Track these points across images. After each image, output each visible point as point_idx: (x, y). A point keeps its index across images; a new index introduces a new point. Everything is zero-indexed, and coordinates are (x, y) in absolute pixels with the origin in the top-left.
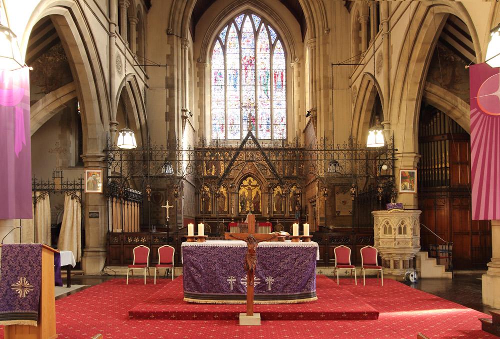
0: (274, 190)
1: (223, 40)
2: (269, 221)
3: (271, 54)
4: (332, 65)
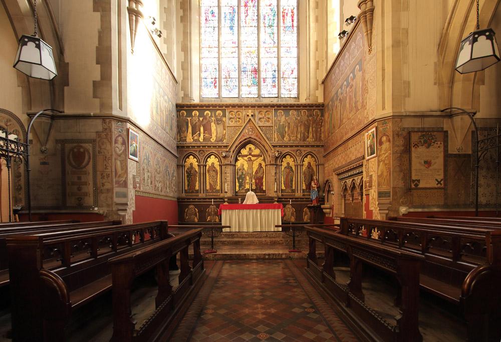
2: (278, 201)
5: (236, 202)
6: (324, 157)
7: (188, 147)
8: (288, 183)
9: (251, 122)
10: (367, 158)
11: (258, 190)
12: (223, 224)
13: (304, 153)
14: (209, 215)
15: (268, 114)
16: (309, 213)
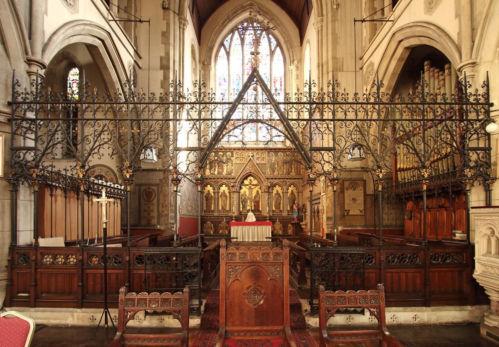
0: (273, 189)
1: (227, 47)
2: (269, 220)
3: (271, 59)
4: (355, 21)
5: (240, 219)
6: (303, 186)
7: (207, 179)
8: (278, 206)
9: (251, 161)
10: (322, 194)
11: (256, 210)
12: (232, 237)
13: (288, 184)
14: (221, 229)
15: (263, 155)
16: (292, 228)
